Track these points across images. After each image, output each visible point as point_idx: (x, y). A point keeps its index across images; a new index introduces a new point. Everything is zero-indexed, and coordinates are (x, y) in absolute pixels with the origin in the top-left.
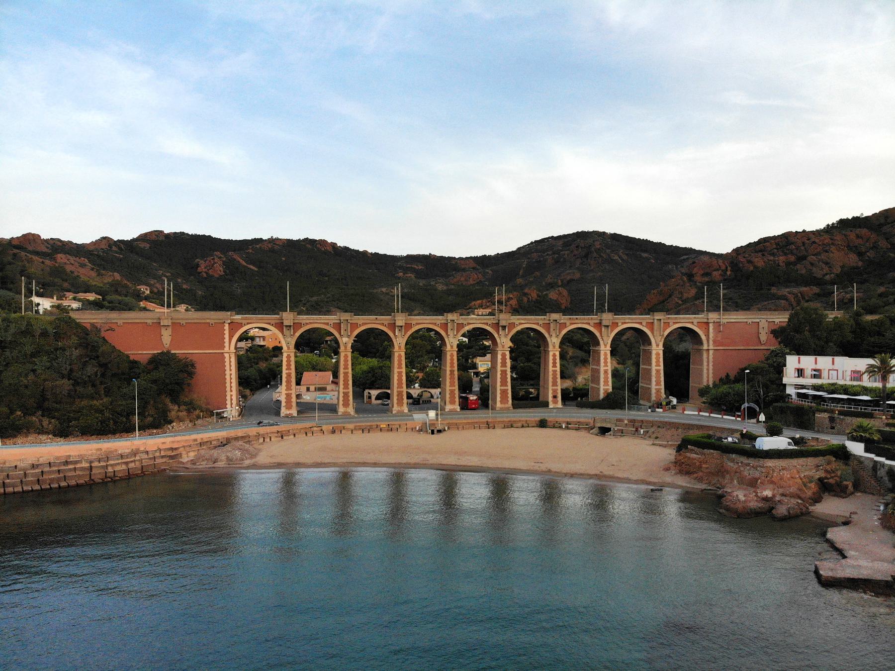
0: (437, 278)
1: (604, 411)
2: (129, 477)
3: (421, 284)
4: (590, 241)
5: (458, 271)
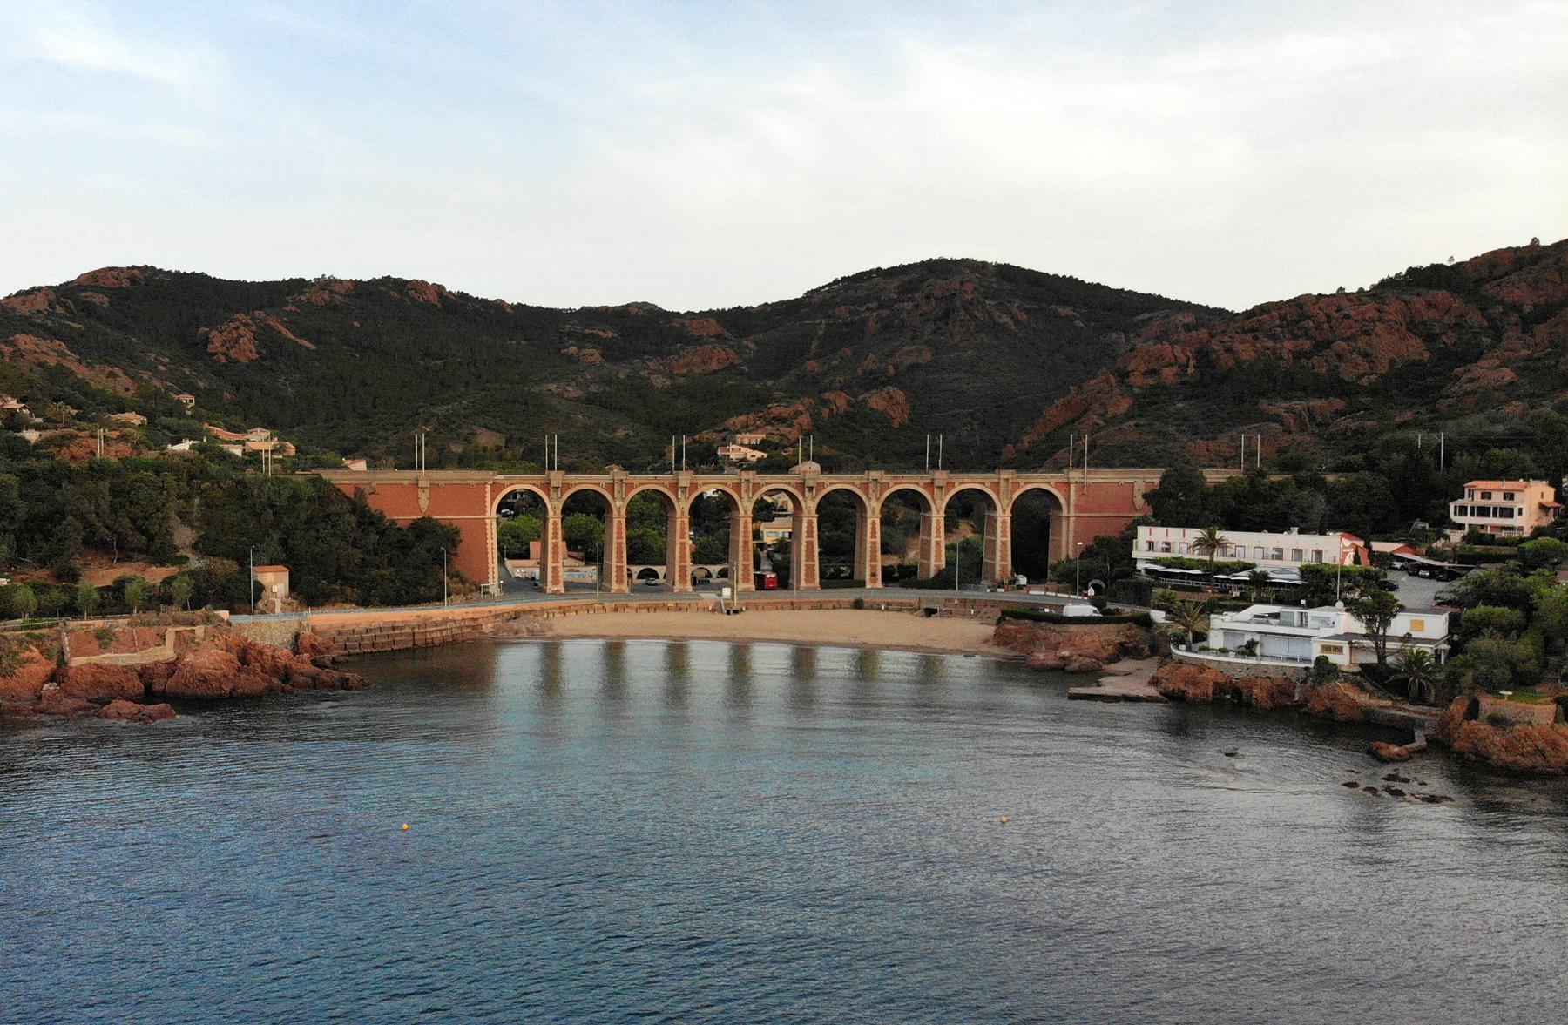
0: (646, 357)
1: (934, 591)
2: (444, 643)
3: (622, 376)
4: (954, 283)
5: (688, 344)
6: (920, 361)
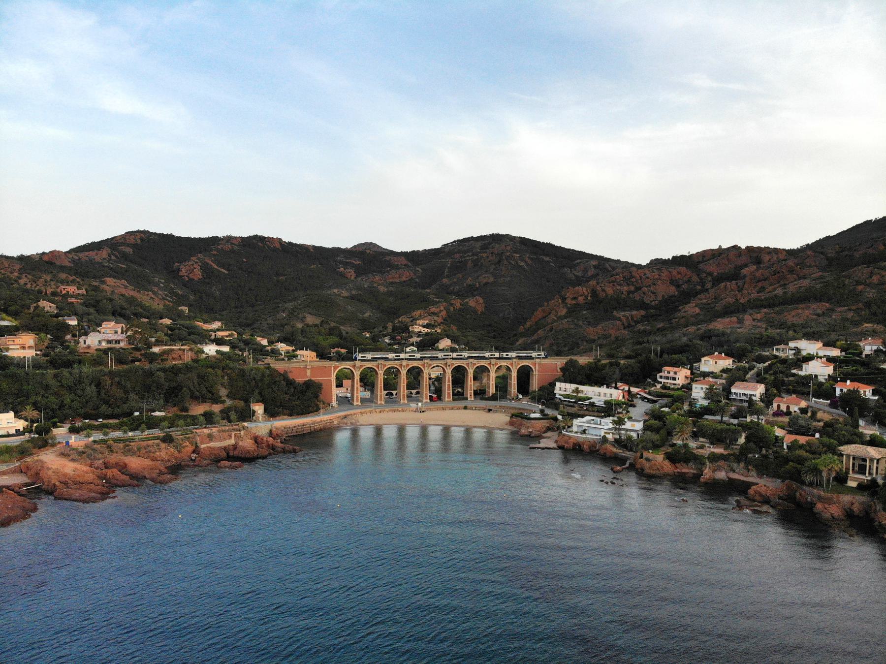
3: (366, 286)
5: (393, 268)
6: (489, 281)
